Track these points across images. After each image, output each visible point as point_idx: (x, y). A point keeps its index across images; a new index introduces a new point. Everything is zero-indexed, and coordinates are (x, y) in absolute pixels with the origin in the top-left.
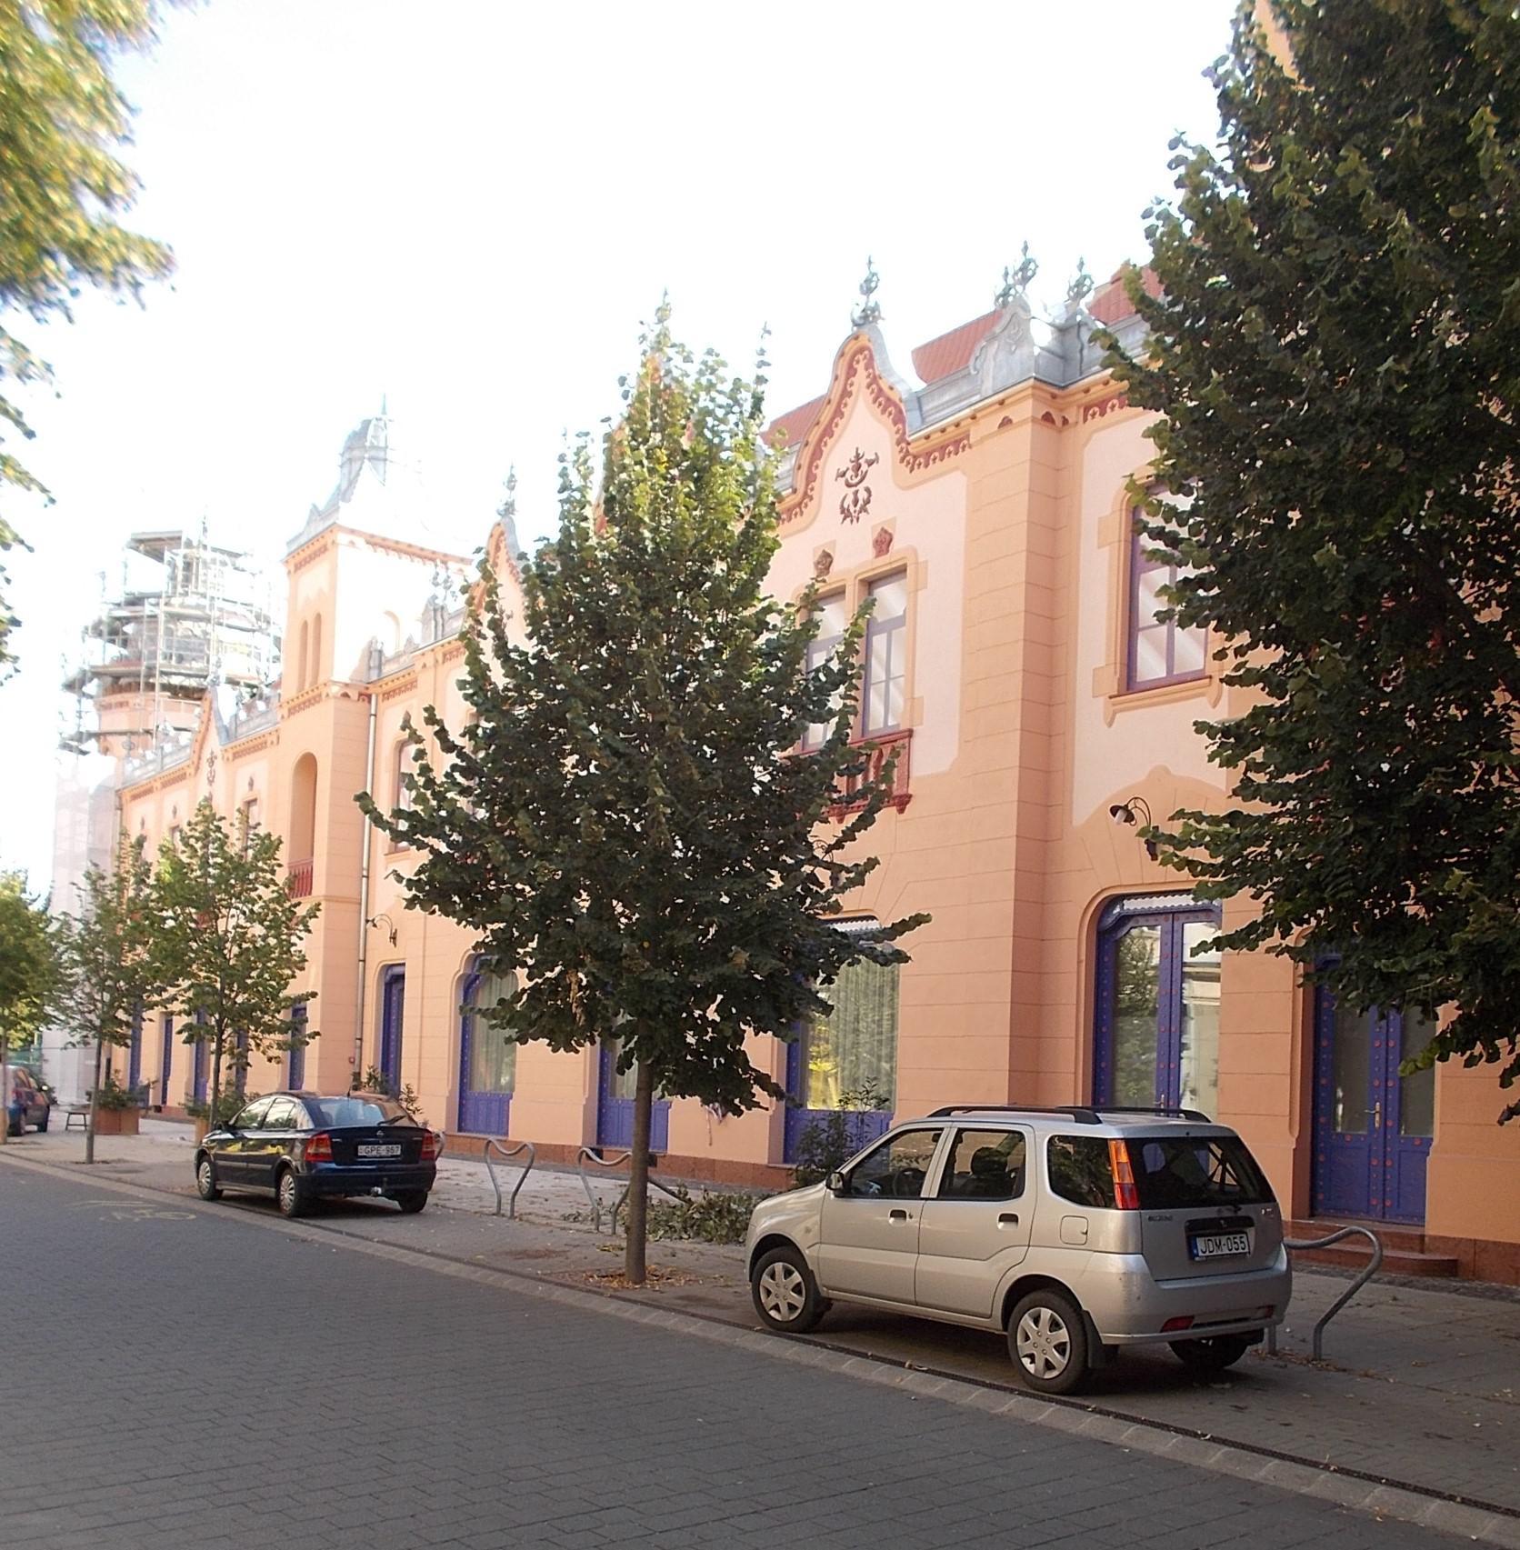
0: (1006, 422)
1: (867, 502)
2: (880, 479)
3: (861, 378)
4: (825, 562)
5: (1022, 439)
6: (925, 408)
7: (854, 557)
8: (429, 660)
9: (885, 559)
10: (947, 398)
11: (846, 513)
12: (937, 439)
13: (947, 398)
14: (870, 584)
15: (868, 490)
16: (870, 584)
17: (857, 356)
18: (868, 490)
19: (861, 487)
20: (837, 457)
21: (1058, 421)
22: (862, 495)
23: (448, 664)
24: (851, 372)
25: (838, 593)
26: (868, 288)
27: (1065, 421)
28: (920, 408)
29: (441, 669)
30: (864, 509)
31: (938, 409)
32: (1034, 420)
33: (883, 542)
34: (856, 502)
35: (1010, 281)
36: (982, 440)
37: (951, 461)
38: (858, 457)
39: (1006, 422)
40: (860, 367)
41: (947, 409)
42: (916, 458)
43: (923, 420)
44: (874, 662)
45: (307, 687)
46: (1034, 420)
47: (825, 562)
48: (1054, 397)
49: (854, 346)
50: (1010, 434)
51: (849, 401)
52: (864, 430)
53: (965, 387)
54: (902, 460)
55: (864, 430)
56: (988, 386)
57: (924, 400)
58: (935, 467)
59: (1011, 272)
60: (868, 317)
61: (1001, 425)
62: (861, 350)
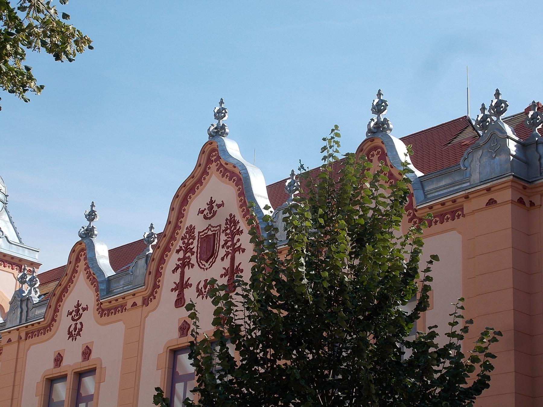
0: (492, 202)
1: (81, 330)
2: (89, 318)
3: (82, 265)
4: (59, 360)
5: (504, 215)
6: (427, 189)
7: (73, 360)
8: (14, 337)
9: (86, 363)
10: (443, 183)
11: (70, 333)
12: (438, 209)
13: (443, 183)
14: (80, 375)
15: (81, 323)
16: (80, 375)
17: (83, 251)
18: (81, 323)
19: (78, 322)
20: (68, 304)
21: (528, 204)
22: (79, 326)
23: (29, 341)
24: (78, 260)
25: (63, 378)
26: (379, 108)
27: (532, 204)
28: (424, 190)
29: (22, 344)
30: (79, 334)
31: (437, 189)
32: (512, 202)
33: (87, 353)
34: (75, 329)
35: (487, 112)
36: (473, 212)
37: (119, 315)
38: (78, 305)
39: (492, 202)
40: (82, 258)
41: (442, 190)
42: (104, 311)
43: (425, 196)
44: (176, 399)
45: (23, 321)
46: (512, 202)
47: (59, 360)
48: (525, 188)
49: (369, 145)
50: (493, 211)
51: (76, 275)
52: (82, 292)
53: (457, 178)
54: (98, 310)
55: (82, 292)
56: (476, 177)
57: (425, 184)
58: (112, 317)
59: (487, 106)
60: (88, 234)
61: (132, 306)
62: (83, 250)
